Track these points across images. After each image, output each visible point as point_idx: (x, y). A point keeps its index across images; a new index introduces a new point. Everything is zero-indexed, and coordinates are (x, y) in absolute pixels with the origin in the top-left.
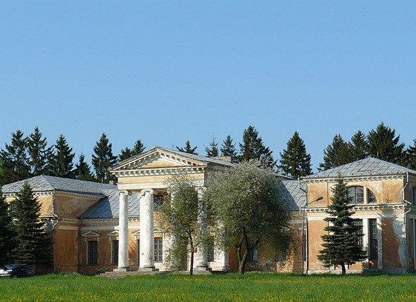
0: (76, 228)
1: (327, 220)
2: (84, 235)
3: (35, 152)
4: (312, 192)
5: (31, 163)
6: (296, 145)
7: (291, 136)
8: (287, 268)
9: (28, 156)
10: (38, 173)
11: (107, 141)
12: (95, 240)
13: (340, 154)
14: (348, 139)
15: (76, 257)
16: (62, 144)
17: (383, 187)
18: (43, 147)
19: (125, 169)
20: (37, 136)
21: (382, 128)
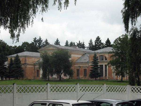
1: (91, 65)
2: (36, 68)
7: (90, 40)
11: (58, 40)
12: (86, 69)
14: (104, 41)
15: (33, 74)
18: (42, 42)
19: (42, 50)
20: (40, 39)
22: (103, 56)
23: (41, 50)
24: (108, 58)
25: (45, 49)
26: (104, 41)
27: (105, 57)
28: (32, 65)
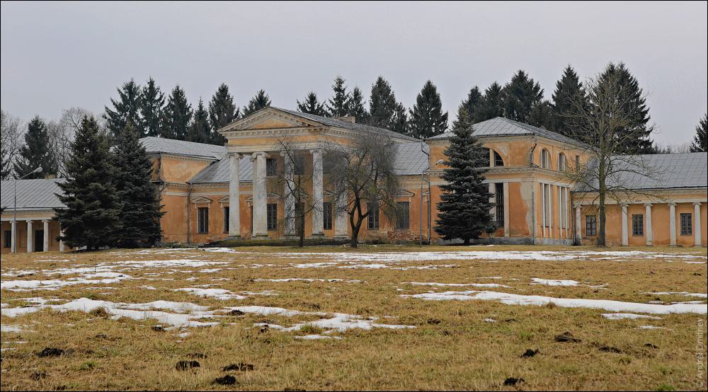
0: (184, 194)
2: (194, 201)
3: (147, 113)
4: (435, 155)
5: (146, 124)
6: (429, 96)
8: (62, 235)
9: (141, 116)
10: (151, 134)
13: (479, 106)
15: (185, 225)
16: (178, 94)
17: (510, 149)
19: (236, 130)
21: (521, 77)
22: (489, 149)
23: (232, 130)
24: (507, 157)
25: (255, 123)
26: (407, 99)
27: (498, 157)
28: (180, 189)
